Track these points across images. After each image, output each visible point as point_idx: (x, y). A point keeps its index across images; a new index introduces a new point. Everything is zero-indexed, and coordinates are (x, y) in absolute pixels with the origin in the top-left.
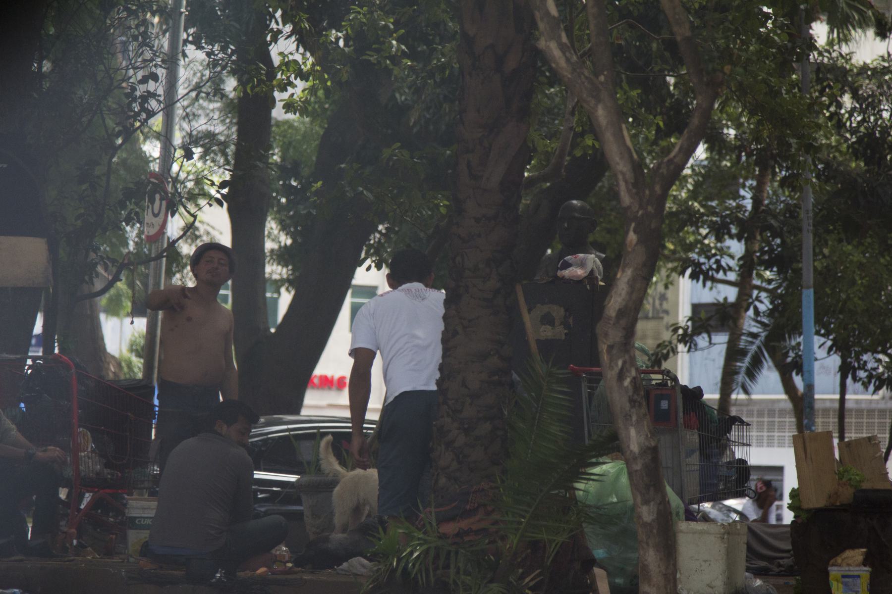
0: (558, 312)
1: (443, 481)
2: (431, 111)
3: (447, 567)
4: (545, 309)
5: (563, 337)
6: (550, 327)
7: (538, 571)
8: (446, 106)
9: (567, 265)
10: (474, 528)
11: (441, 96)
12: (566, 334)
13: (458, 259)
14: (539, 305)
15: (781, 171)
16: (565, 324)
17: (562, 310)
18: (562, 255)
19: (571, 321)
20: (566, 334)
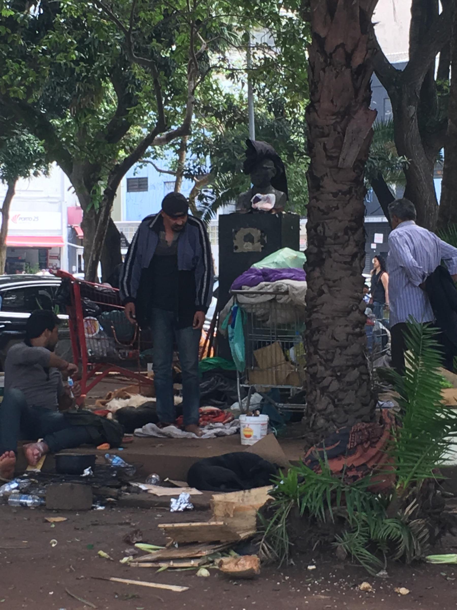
0: (256, 233)
1: (321, 422)
2: (50, 91)
3: (344, 503)
4: (247, 231)
5: (260, 250)
6: (251, 244)
7: (415, 500)
8: (58, 89)
9: (257, 200)
10: (356, 464)
11: (55, 83)
12: (262, 248)
13: (320, 228)
14: (242, 229)
15: (149, 111)
16: (262, 242)
17: (259, 231)
18: (253, 192)
19: (265, 238)
20: (262, 248)
